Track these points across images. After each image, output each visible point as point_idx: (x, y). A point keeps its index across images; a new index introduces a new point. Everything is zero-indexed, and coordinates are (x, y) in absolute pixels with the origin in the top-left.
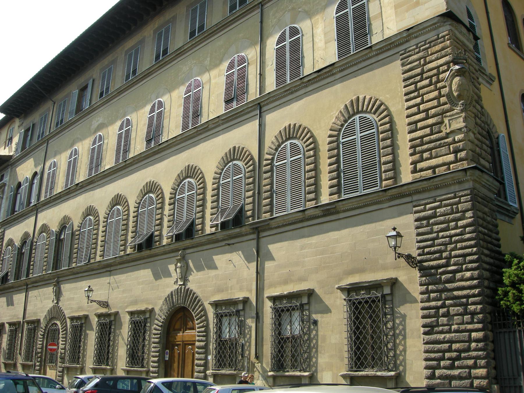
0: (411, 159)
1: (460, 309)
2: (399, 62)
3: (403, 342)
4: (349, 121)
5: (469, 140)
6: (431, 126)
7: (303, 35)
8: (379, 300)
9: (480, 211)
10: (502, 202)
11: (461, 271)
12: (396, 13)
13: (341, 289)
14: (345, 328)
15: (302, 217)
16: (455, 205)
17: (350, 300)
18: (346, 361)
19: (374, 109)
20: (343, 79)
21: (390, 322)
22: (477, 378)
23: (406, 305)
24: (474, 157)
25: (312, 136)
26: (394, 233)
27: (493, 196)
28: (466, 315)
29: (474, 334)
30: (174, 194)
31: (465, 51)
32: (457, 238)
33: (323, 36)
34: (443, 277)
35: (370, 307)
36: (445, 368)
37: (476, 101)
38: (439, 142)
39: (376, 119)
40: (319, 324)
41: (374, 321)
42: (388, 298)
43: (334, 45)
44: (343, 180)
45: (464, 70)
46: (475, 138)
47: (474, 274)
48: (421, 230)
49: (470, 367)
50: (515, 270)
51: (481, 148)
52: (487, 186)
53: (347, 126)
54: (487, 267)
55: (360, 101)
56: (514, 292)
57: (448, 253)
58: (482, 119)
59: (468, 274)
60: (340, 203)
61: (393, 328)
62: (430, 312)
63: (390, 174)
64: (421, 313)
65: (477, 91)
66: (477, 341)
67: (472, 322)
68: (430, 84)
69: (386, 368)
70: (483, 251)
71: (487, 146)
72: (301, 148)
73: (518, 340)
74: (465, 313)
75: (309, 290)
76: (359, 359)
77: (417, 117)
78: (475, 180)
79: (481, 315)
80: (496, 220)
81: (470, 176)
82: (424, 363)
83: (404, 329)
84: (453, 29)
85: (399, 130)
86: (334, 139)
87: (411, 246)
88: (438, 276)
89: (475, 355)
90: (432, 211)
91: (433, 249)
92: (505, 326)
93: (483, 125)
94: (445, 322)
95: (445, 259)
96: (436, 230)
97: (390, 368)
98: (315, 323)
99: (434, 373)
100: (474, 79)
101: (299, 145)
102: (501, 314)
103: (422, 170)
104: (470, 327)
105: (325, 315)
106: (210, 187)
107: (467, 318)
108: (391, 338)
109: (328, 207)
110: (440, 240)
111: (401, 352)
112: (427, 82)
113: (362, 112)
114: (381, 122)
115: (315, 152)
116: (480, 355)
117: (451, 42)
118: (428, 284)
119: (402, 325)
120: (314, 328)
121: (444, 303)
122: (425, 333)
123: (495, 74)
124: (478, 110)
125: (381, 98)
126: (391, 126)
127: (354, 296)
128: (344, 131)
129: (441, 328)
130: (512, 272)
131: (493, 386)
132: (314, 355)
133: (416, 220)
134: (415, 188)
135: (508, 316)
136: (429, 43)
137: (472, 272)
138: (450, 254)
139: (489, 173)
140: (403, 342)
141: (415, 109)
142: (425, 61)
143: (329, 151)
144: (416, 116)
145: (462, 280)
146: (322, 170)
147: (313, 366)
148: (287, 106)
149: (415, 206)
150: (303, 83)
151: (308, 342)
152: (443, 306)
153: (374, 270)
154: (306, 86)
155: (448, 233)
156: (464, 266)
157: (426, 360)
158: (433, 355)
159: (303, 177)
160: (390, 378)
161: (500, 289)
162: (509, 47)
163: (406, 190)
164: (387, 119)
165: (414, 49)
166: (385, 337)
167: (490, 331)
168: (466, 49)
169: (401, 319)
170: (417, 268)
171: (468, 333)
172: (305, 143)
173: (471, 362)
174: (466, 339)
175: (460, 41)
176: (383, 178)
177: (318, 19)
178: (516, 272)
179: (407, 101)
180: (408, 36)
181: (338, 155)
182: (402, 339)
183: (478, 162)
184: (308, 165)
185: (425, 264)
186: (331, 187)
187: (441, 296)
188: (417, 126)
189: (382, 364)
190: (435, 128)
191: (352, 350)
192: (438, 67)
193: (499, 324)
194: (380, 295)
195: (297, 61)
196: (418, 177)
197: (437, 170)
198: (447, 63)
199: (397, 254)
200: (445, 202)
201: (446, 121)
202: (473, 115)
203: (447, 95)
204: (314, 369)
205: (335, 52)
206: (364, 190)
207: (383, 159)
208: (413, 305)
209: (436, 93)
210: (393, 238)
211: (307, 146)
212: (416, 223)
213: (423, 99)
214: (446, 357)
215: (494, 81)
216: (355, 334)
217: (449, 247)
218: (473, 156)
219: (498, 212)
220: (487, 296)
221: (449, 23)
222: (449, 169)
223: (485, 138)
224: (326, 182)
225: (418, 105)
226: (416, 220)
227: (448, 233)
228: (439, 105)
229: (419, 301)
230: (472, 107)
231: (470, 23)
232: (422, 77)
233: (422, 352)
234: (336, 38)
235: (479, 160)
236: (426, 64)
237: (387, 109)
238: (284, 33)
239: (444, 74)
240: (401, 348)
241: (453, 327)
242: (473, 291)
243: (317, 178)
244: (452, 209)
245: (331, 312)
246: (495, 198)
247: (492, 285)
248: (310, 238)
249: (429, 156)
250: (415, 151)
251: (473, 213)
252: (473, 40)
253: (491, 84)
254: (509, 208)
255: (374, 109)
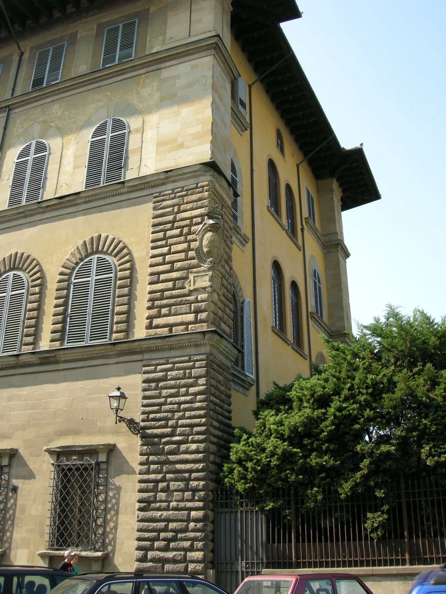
0: (147, 313)
1: (181, 485)
2: (151, 205)
3: (114, 518)
4: (85, 261)
5: (212, 302)
6: (174, 280)
7: (50, 154)
8: (92, 468)
9: (213, 379)
10: (239, 372)
11: (185, 442)
12: (157, 151)
13: (50, 452)
14: (49, 498)
15: (14, 362)
16: (188, 369)
17: (59, 466)
18: (47, 537)
19: (115, 251)
20: (86, 212)
21: (102, 495)
22: (193, 562)
23: (122, 476)
24: (215, 320)
25: (41, 270)
26: (118, 394)
27: (229, 364)
28: (187, 491)
29: (193, 513)
30: (66, 278)
31: (223, 206)
32: (186, 406)
33: (72, 159)
34: (167, 447)
35: (81, 475)
36: (159, 549)
37: (225, 260)
38: (180, 299)
39: (116, 263)
40: (19, 491)
41: (84, 492)
42: (103, 466)
43: (83, 173)
44: (68, 326)
45: (218, 225)
46: (219, 300)
47: (200, 446)
48: (148, 393)
49: (186, 550)
50: (243, 446)
51: (224, 312)
52: (225, 353)
53: (83, 265)
54: (215, 440)
55: (101, 240)
56: (240, 469)
57: (174, 421)
58: (229, 281)
59: (194, 447)
60: (61, 352)
61: (105, 501)
62: (148, 486)
63: (123, 326)
64: (138, 486)
65: (229, 250)
66: (196, 520)
67: (192, 500)
68: (180, 235)
69: (93, 547)
70: (212, 423)
71: (231, 310)
72: (26, 283)
73: (239, 521)
74: (186, 489)
75: (12, 450)
76: (62, 535)
77: (161, 268)
78: (213, 345)
79: (203, 493)
80: (230, 390)
81: (207, 340)
82: (136, 543)
83: (118, 503)
84: (214, 180)
85: (139, 279)
86: (66, 277)
87: (135, 410)
88: (161, 446)
89: (192, 536)
90: (162, 373)
91: (158, 415)
92: (227, 505)
93: (229, 287)
94: (164, 498)
95: (170, 427)
96: (165, 395)
97: (97, 547)
98: (15, 489)
99: (146, 555)
100: (227, 237)
101: (24, 278)
102: (224, 493)
103: (157, 327)
104: (190, 504)
105: (27, 481)
106: (52, 285)
107: (188, 494)
108: (102, 513)
109: (46, 355)
110: (168, 406)
111: (111, 529)
112: (177, 231)
113: (102, 252)
114: (121, 267)
115: (41, 290)
116: (198, 537)
117: (209, 194)
118: (149, 454)
119: (116, 499)
120: (13, 496)
121: (165, 476)
122: (140, 509)
123: (249, 235)
124: (226, 271)
125: (125, 240)
126: (131, 273)
127: (65, 462)
128: (78, 271)
129: (158, 505)
130: (239, 448)
131: (208, 571)
132: (9, 529)
133: (144, 382)
134: (149, 346)
135: (231, 494)
136: (186, 190)
137: (198, 444)
138: (177, 423)
139: (229, 339)
140: (114, 518)
141: (160, 259)
142: (179, 209)
143: (57, 290)
144: (160, 267)
145: (186, 452)
146: (46, 311)
147: (6, 541)
148: (17, 230)
149: (145, 366)
150: (40, 208)
151: (3, 512)
152: (163, 480)
153: (90, 433)
154: (43, 212)
155: (177, 399)
156: (190, 437)
157: (139, 539)
158: (147, 535)
159: (22, 316)
160: (96, 559)
161: (225, 465)
162: (268, 210)
163: (138, 347)
164: (128, 265)
165: (169, 194)
166: (95, 512)
167: (212, 510)
168: (224, 204)
169: (115, 492)
170: (139, 435)
171: (187, 512)
172: (31, 276)
173: (187, 544)
174: (185, 518)
175: (219, 194)
176: (114, 329)
177: (71, 139)
178: (244, 448)
179: (153, 248)
180: (166, 178)
181: (67, 297)
182: (115, 515)
183: (219, 327)
184: (31, 302)
185: (148, 431)
186: (53, 332)
187: (162, 468)
188: (159, 277)
189: (88, 542)
190: (179, 284)
191: (55, 524)
192: (191, 218)
193: (221, 502)
194: (94, 462)
195: (38, 182)
196: (153, 334)
197: (174, 328)
198: (202, 216)
199: (118, 418)
200: (178, 365)
201: (191, 277)
202: (221, 276)
203: (196, 249)
204: (7, 545)
205: (83, 179)
206: (90, 340)
207: (117, 309)
208: (130, 476)
209: (185, 245)
210: (115, 399)
211: (33, 281)
212: (144, 385)
213: (170, 249)
214: (161, 538)
215: (247, 243)
216: (61, 505)
217: (177, 415)
218: (214, 319)
219: (233, 381)
220: (212, 472)
221: (211, 174)
222: (187, 329)
223: (229, 301)
224: (48, 325)
225: (164, 255)
226: (144, 382)
227: (177, 399)
228: (186, 259)
229: (137, 472)
230: (220, 266)
231: (232, 178)
232: (173, 226)
233: (135, 531)
234: (87, 165)
235: (220, 324)
236: (179, 212)
237: (129, 253)
238: (29, 147)
239: (196, 227)
240: (112, 524)
241: (172, 504)
242: (197, 465)
243: (38, 319)
244: (185, 373)
245: (34, 477)
246: (232, 367)
247: (218, 460)
248: (21, 389)
249: (168, 312)
250: (153, 304)
251: (206, 381)
252: (232, 196)
253: (244, 245)
254: (245, 379)
255: (115, 251)
